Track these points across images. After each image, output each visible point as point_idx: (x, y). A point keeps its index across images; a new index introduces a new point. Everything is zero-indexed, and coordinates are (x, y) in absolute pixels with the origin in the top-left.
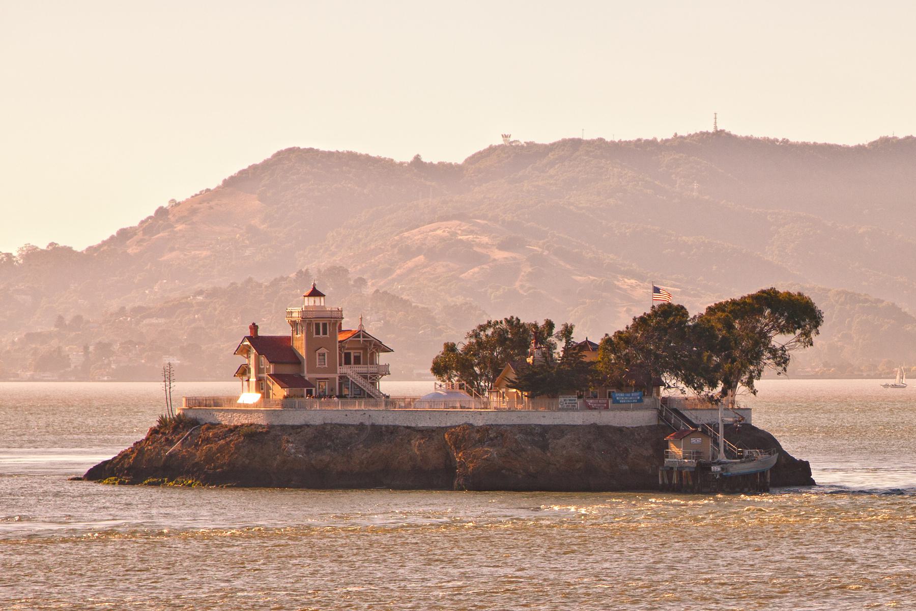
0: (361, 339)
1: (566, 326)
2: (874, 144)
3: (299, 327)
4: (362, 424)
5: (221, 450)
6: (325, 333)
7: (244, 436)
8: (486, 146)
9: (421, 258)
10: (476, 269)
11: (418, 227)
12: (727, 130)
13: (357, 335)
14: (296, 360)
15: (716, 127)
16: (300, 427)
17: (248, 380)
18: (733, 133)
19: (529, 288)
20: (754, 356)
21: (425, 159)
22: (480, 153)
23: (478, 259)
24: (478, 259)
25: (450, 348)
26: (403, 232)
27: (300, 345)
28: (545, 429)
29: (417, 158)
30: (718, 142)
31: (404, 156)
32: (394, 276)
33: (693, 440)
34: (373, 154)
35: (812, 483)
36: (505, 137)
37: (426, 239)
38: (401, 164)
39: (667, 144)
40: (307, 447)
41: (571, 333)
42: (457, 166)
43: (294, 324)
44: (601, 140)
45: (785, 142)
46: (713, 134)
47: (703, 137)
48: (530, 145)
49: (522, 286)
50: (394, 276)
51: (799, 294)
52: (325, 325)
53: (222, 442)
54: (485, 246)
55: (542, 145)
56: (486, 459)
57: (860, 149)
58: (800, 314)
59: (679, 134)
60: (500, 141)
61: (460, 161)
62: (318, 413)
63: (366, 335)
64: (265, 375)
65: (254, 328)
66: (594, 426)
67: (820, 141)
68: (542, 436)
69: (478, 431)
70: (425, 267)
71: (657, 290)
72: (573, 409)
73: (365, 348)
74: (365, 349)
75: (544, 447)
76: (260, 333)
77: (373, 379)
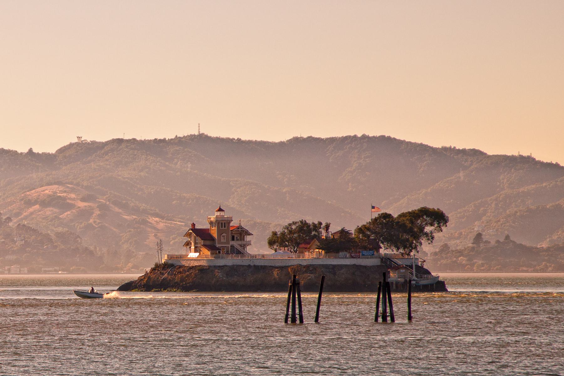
0: (240, 230)
1: (327, 223)
2: (290, 141)
3: (214, 224)
4: (249, 265)
5: (187, 276)
6: (225, 227)
7: (199, 270)
8: (68, 143)
9: (37, 207)
10: (69, 213)
11: (34, 189)
12: (206, 134)
13: (238, 228)
14: (212, 239)
15: (199, 132)
16: (223, 266)
17: (190, 248)
18: (209, 135)
19: (99, 223)
20: (417, 237)
21: (35, 151)
22: (64, 147)
23: (70, 207)
24: (70, 207)
25: (275, 234)
26: (25, 192)
27: (214, 232)
28: (334, 266)
29: (31, 150)
30: (201, 140)
31: (23, 149)
32: (22, 216)
33: (402, 271)
34: (6, 148)
35: (446, 290)
36: (79, 138)
37: (39, 195)
38: (21, 153)
39: (172, 141)
40: (227, 275)
41: (329, 226)
42: (52, 154)
43: (211, 223)
44: (134, 139)
45: (239, 140)
46: (198, 136)
47: (192, 138)
48: (93, 143)
49: (95, 222)
50: (22, 216)
51: (438, 209)
52: (225, 223)
53: (187, 273)
54: (74, 199)
55: (100, 142)
56: (310, 279)
57: (282, 144)
58: (439, 218)
59: (178, 136)
60: (75, 140)
61: (54, 152)
62: (230, 261)
63: (242, 228)
64: (199, 245)
65: (194, 225)
66: (354, 265)
67: (259, 139)
68: (334, 269)
69: (304, 267)
70: (40, 211)
71: (373, 207)
72: (346, 258)
73: (241, 233)
74: (241, 234)
75: (335, 274)
76: (197, 227)
77: (244, 246)
